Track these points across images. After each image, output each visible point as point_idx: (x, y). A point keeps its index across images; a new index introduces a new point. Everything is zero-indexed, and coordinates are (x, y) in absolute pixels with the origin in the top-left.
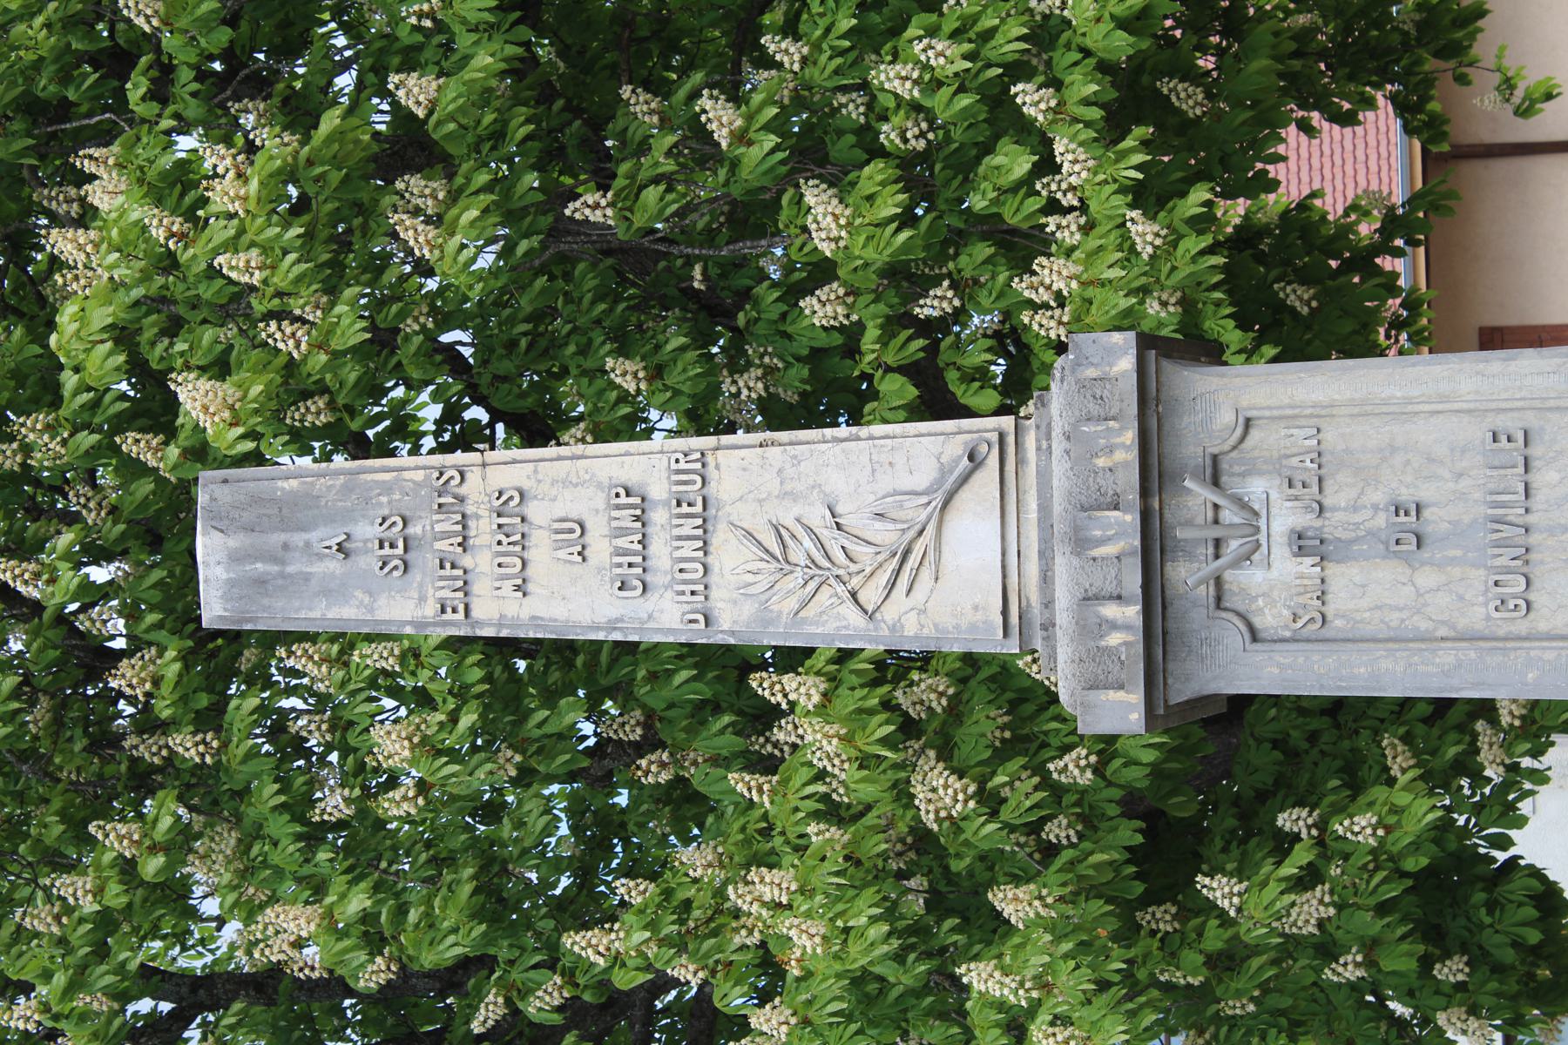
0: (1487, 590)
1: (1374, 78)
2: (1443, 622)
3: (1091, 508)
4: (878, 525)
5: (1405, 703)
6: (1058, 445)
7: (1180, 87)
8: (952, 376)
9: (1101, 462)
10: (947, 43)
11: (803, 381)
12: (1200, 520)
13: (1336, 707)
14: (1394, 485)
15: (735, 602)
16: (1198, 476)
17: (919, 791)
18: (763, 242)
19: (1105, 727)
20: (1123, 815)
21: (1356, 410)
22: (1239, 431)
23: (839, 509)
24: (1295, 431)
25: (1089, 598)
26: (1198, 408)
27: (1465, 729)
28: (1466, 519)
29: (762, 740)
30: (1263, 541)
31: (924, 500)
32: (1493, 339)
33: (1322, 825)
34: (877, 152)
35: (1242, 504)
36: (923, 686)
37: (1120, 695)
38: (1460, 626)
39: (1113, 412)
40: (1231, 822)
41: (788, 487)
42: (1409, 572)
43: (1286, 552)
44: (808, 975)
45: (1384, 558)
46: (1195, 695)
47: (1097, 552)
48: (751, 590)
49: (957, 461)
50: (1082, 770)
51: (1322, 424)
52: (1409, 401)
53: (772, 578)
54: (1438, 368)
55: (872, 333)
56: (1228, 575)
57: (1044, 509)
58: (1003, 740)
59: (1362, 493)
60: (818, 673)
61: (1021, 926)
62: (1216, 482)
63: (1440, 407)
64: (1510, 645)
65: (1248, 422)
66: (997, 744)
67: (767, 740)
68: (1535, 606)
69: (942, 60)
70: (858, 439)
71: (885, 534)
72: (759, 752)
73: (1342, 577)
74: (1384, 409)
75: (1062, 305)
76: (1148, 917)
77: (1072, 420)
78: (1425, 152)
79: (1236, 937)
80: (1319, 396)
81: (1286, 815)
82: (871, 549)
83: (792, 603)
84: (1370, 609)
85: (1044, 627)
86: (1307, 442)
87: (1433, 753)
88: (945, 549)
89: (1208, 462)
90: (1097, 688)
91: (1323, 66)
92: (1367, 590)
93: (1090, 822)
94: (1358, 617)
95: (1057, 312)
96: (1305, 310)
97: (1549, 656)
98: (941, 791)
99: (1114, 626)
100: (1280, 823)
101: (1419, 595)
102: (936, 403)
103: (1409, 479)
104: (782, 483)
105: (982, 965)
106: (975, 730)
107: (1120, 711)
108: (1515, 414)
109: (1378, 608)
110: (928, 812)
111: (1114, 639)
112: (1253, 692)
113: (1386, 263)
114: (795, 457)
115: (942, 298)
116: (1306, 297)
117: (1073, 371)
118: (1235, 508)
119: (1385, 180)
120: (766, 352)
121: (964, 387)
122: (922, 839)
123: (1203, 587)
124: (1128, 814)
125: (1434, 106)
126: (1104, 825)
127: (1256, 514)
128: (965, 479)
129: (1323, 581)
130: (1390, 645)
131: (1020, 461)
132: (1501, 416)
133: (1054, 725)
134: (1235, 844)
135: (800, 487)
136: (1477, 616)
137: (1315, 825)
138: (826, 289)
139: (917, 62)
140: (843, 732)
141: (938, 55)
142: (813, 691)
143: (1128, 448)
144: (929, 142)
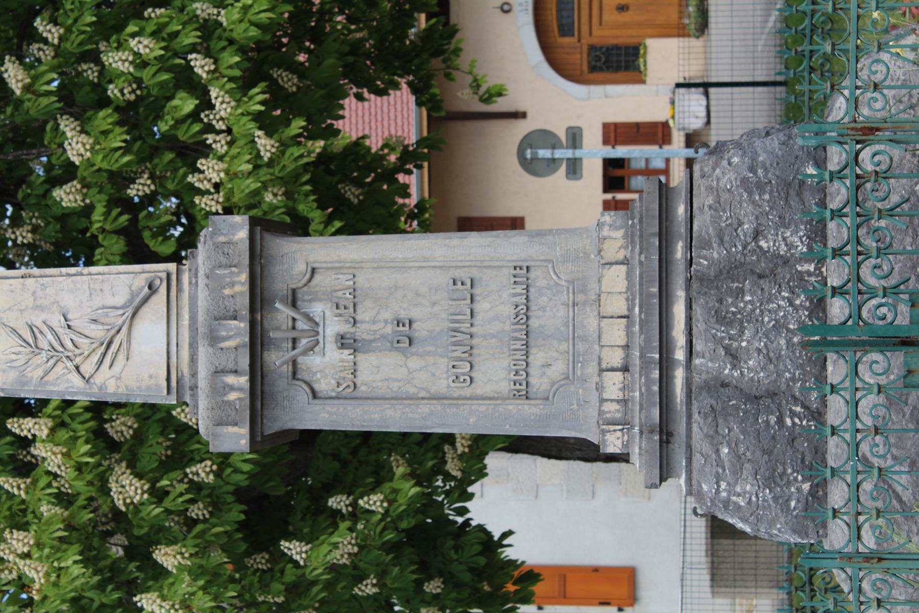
0: (448, 371)
1: (399, 72)
2: (423, 389)
3: (220, 319)
4: (93, 326)
5: (405, 435)
6: (202, 281)
7: (284, 74)
8: (146, 234)
9: (227, 292)
10: (150, 40)
11: (57, 232)
12: (284, 327)
13: (366, 436)
14: (397, 309)
15: (4, 371)
16: (284, 301)
17: (113, 486)
18: (34, 151)
19: (225, 448)
20: (235, 501)
21: (376, 265)
22: (308, 276)
23: (69, 316)
24: (340, 276)
25: (219, 372)
26: (285, 261)
27: (438, 448)
28: (437, 329)
29: (24, 453)
30: (321, 340)
31: (121, 312)
32: (467, 224)
33: (354, 504)
34: (104, 102)
35: (309, 318)
36: (118, 422)
37: (235, 429)
38: (432, 391)
39: (235, 262)
40: (306, 503)
41: (38, 302)
42: (404, 359)
43: (334, 346)
44: (45, 598)
45: (390, 351)
46: (280, 430)
47: (224, 345)
48: (14, 364)
49: (143, 287)
50: (208, 474)
51: (357, 274)
53: (27, 357)
54: (423, 242)
55: (100, 210)
56: (300, 360)
58: (167, 456)
59: (378, 313)
60: (49, 416)
61: (174, 571)
62: (294, 305)
63: (424, 264)
64: (460, 402)
65: (313, 271)
66: (163, 458)
67: (29, 453)
68: (475, 380)
69: (147, 50)
70: (82, 274)
71: (98, 332)
72: (22, 460)
73: (366, 361)
74: (392, 264)
75: (218, 192)
76: (252, 562)
77: (210, 267)
78: (429, 117)
79: (304, 575)
80: (354, 256)
81: (333, 499)
82: (88, 341)
83: (40, 372)
84: (381, 381)
85: (191, 389)
86: (347, 283)
87: (420, 464)
88: (133, 342)
89: (290, 293)
90: (222, 425)
91: (368, 62)
92: (380, 370)
93: (217, 507)
94: (374, 385)
95: (216, 196)
96: (356, 201)
97: (483, 408)
98: (127, 488)
99: (232, 388)
100: (330, 504)
101: (410, 373)
102: (136, 253)
103: (405, 305)
104: (35, 300)
105: (149, 595)
106: (150, 450)
107: (235, 439)
108: (466, 269)
109: (386, 380)
110: (119, 499)
111: (233, 396)
112: (313, 428)
113: (402, 178)
114: (43, 285)
115: (143, 185)
116: (357, 193)
117: (211, 238)
118: (305, 321)
119: (406, 130)
120: (34, 216)
121: (154, 241)
122: (117, 515)
123: (285, 366)
124: (239, 501)
125: (435, 90)
126: (225, 508)
127: (317, 324)
128: (146, 300)
129: (355, 364)
130: (393, 402)
131: (179, 290)
132: (458, 271)
133: (197, 446)
134: (308, 516)
135: (45, 302)
136: (442, 385)
137: (350, 505)
138: (69, 185)
139: (131, 50)
140: (64, 450)
141: (146, 47)
142: (43, 427)
143: (243, 284)
144: (137, 96)
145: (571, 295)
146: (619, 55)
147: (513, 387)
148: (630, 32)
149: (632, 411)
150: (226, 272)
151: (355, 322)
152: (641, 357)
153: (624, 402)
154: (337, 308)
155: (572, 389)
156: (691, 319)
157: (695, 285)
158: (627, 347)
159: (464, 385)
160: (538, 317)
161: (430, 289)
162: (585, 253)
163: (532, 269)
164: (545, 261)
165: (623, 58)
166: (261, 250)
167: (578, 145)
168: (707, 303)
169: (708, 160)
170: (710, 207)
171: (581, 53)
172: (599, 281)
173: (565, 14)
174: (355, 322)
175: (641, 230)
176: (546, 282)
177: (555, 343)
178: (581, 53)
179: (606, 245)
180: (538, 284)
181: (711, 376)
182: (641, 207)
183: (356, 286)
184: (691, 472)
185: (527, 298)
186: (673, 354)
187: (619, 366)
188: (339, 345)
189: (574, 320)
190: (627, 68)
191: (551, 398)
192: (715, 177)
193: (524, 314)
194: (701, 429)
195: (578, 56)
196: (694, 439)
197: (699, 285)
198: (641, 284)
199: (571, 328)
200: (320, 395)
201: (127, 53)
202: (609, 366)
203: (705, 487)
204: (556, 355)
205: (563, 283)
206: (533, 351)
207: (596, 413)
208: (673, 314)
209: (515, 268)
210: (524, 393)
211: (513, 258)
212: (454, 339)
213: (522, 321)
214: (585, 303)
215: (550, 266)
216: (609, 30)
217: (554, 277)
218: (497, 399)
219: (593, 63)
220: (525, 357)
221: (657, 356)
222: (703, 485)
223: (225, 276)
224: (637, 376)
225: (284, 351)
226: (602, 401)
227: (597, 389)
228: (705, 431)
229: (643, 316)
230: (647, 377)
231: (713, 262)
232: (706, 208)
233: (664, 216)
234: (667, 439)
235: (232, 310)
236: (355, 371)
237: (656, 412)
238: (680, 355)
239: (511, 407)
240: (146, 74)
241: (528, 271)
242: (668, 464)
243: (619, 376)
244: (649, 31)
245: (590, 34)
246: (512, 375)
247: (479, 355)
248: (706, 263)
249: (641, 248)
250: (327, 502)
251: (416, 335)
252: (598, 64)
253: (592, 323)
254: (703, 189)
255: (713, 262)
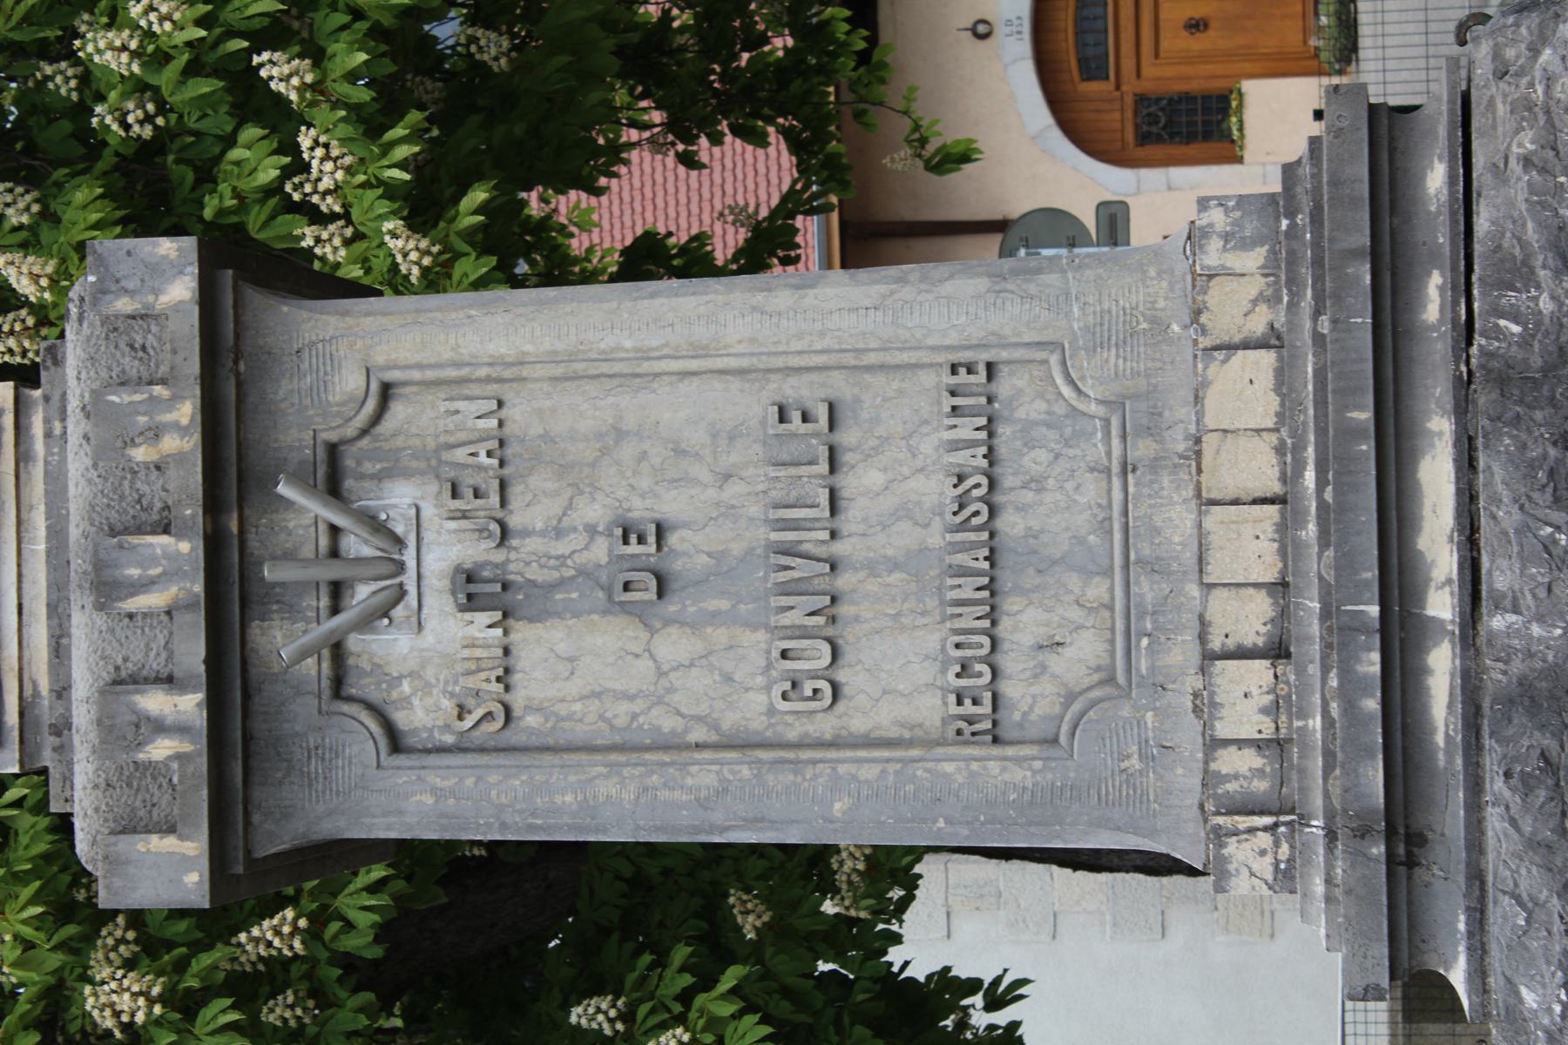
0: (769, 666)
2: (699, 719)
3: (127, 531)
6: (76, 427)
9: (140, 454)
12: (307, 552)
14: (621, 494)
16: (301, 478)
21: (559, 370)
22: (371, 405)
25: (123, 681)
28: (737, 549)
34: (91, 144)
35: (376, 525)
37: (169, 843)
39: (163, 370)
42: (644, 635)
43: (448, 604)
45: (605, 613)
47: (132, 604)
51: (508, 396)
52: (644, 355)
56: (354, 642)
57: (57, 534)
59: (570, 506)
62: (334, 489)
63: (694, 365)
64: (806, 755)
65: (387, 392)
68: (846, 690)
73: (538, 644)
74: (605, 368)
81: (580, 1010)
84: (582, 698)
86: (481, 423)
89: (321, 454)
90: (134, 831)
92: (577, 667)
94: (562, 710)
99: (159, 727)
100: (573, 1019)
101: (661, 674)
108: (814, 377)
111: (161, 749)
127: (399, 542)
129: (507, 651)
132: (793, 381)
136: (752, 708)
143: (183, 431)
144: (156, 127)
145: (1116, 442)
146: (1193, 111)
147: (954, 709)
148: (1210, 69)
149: (1302, 771)
150: (137, 397)
151: (505, 533)
152: (1325, 614)
153: (1276, 746)
154: (455, 494)
155: (1126, 711)
156: (1473, 498)
157: (1484, 398)
158: (1281, 588)
159: (813, 705)
160: (1022, 509)
161: (714, 436)
162: (1154, 321)
163: (1004, 371)
164: (1039, 345)
165: (1199, 118)
166: (237, 336)
167: (1120, 237)
168: (1523, 447)
169: (1517, 25)
170: (1527, 162)
171: (1122, 110)
172: (1198, 399)
173: (1090, 38)
174: (505, 533)
175: (1317, 244)
176: (1043, 406)
177: (1073, 581)
178: (1122, 110)
179: (1216, 294)
180: (1021, 414)
181: (1539, 665)
182: (1316, 176)
183: (507, 430)
184: (1485, 951)
185: (990, 455)
186: (1421, 601)
187: (1260, 641)
188: (462, 598)
189: (1125, 513)
190: (1207, 136)
191: (1063, 739)
192: (1538, 74)
193: (981, 500)
194: (1513, 822)
195: (1117, 115)
196: (1491, 856)
197: (1495, 395)
198: (1320, 403)
199: (1118, 536)
200: (411, 741)
201: (126, 33)
202: (1231, 643)
203: (1530, 998)
204: (1076, 614)
205: (1093, 408)
206: (1010, 604)
207: (1196, 782)
208: (1417, 483)
209: (954, 369)
210: (987, 725)
211: (948, 342)
212: (783, 576)
213: (975, 521)
214: (1155, 465)
215: (1054, 360)
216: (1173, 66)
217: (1066, 391)
218: (910, 744)
219: (1145, 128)
220: (986, 623)
221: (1374, 610)
222: (1524, 991)
223: (134, 408)
224: (1314, 669)
225: (308, 621)
226: (1214, 744)
227: (1197, 710)
228: (1528, 829)
229: (1328, 495)
230: (1346, 673)
231: (1538, 324)
232: (1515, 166)
233: (1385, 198)
234: (1409, 854)
235: (158, 505)
236: (507, 671)
237: (1374, 776)
238: (1441, 605)
239: (949, 767)
240: (166, 78)
241: (990, 377)
242: (1412, 927)
243: (1259, 673)
244: (1248, 67)
245: (1138, 75)
246: (951, 676)
247: (857, 619)
248: (1516, 329)
249: (1319, 298)
250: (569, 1014)
251: (677, 565)
252: (1154, 129)
253: (1178, 520)
254: (1501, 109)
255: (1538, 324)
